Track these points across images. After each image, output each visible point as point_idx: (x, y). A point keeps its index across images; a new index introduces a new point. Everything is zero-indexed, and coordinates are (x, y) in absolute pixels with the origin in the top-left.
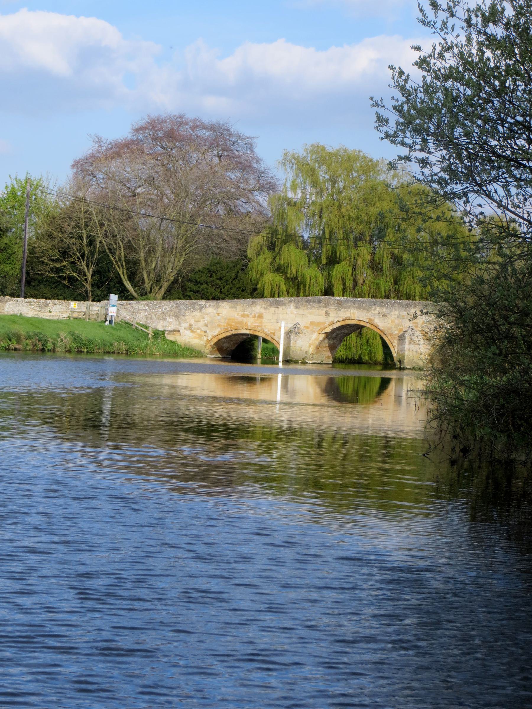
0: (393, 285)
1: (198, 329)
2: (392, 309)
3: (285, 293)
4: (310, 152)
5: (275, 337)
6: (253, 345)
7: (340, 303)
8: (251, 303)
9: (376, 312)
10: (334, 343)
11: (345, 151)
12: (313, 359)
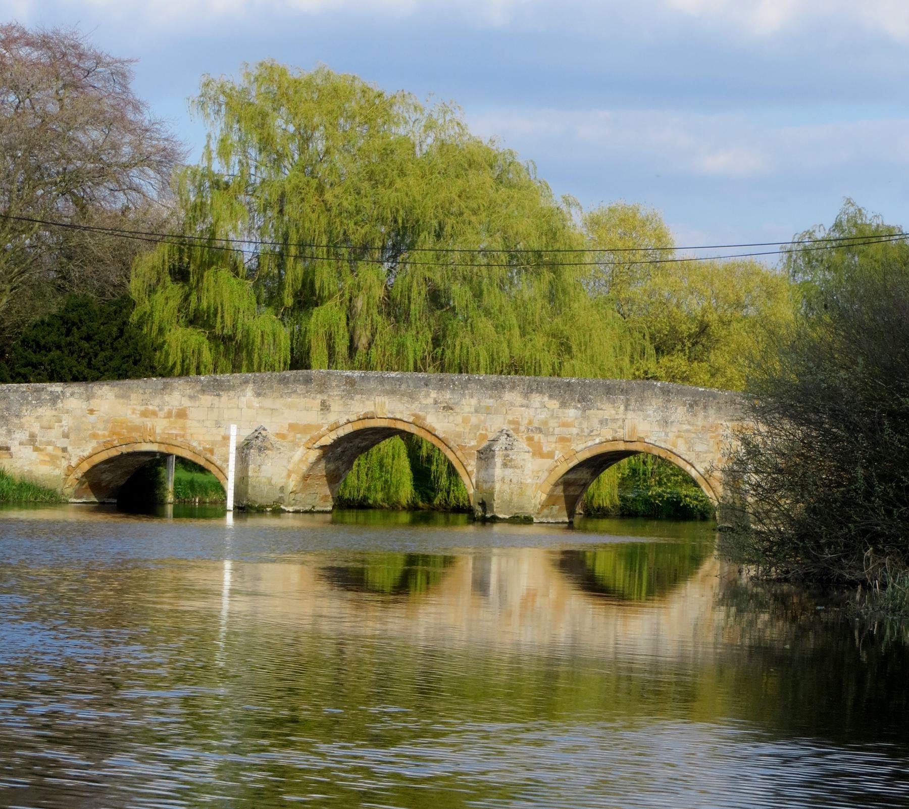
0: (431, 346)
1: (49, 443)
2: (463, 395)
3: (211, 367)
4: (256, 79)
5: (215, 459)
6: (158, 474)
7: (351, 382)
8: (160, 386)
9: (430, 401)
10: (337, 469)
11: (327, 77)
12: (296, 502)
